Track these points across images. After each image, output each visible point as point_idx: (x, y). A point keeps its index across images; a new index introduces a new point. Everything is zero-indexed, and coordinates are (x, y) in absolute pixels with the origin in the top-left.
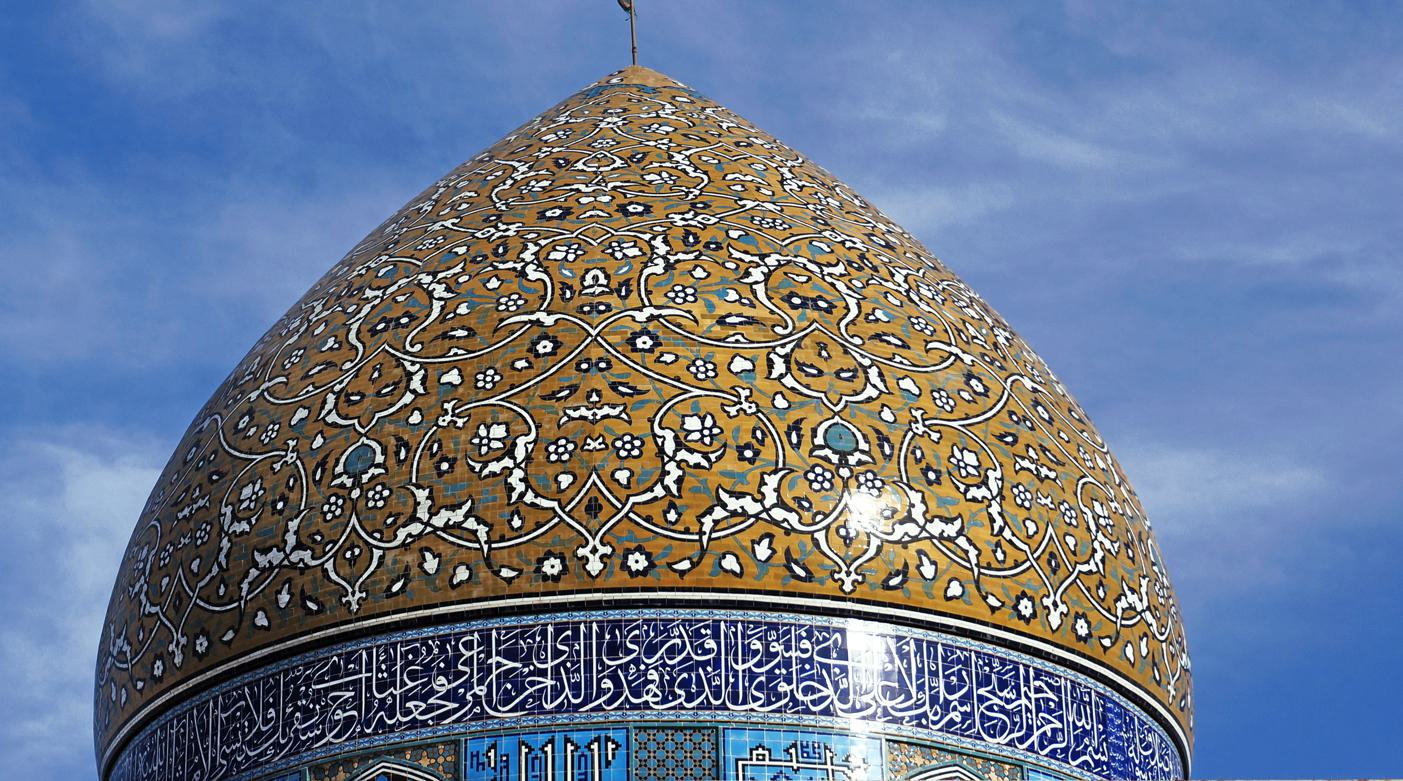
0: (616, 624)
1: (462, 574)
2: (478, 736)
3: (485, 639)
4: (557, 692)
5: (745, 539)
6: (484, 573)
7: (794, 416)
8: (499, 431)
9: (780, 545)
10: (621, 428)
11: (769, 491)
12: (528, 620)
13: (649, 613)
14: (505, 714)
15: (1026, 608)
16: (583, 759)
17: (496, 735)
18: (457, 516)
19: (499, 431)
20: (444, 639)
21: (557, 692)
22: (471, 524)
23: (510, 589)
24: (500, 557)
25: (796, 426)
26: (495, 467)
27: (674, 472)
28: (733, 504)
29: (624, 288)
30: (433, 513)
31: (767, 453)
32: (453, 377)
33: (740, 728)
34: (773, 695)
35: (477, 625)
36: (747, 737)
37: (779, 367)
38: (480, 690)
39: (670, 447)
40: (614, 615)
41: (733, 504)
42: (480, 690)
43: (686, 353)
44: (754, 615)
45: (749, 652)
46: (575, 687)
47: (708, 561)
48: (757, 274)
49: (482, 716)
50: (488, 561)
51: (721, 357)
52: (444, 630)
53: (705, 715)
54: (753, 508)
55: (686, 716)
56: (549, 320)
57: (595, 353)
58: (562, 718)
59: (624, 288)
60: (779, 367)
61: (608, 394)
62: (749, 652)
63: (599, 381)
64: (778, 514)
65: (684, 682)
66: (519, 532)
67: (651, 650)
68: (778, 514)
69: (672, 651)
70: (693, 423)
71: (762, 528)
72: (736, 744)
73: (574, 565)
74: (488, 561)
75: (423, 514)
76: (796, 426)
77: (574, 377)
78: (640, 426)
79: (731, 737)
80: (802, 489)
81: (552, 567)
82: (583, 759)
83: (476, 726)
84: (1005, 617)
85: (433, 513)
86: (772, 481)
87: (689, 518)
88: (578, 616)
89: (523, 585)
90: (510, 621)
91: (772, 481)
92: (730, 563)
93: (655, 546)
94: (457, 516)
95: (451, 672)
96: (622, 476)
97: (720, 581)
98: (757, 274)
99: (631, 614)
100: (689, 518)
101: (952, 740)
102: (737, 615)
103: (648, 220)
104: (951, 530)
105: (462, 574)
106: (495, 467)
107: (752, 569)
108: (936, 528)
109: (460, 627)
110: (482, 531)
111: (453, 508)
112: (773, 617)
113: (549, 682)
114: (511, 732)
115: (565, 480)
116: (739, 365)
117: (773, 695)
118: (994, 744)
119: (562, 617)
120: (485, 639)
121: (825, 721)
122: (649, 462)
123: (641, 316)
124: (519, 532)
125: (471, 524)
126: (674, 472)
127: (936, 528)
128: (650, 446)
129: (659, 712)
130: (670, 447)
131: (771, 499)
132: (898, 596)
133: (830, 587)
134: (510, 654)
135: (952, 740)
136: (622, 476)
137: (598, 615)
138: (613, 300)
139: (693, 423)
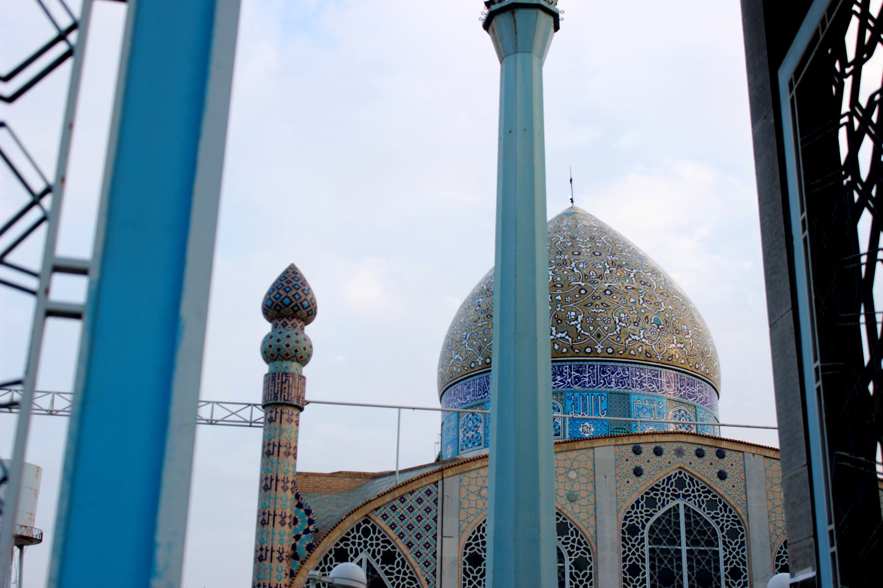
0: (604, 366)
1: (565, 350)
2: (569, 392)
3: (570, 367)
4: (589, 382)
5: (636, 346)
6: (570, 350)
7: (646, 315)
8: (573, 314)
9: (644, 348)
10: (605, 315)
11: (641, 334)
12: (581, 363)
13: (612, 364)
14: (576, 387)
15: (697, 366)
16: (596, 400)
17: (573, 392)
18: (563, 335)
19: (573, 314)
20: (559, 366)
21: (589, 382)
22: (567, 337)
23: (577, 355)
24: (575, 347)
25: (647, 318)
26: (573, 323)
27: (619, 328)
28: (633, 337)
29: (600, 277)
30: (557, 333)
31: (641, 324)
32: (559, 298)
33: (635, 394)
34: (642, 386)
35: (568, 363)
36: (636, 397)
37: (641, 302)
38: (569, 380)
39: (617, 321)
40: (603, 363)
41: (633, 337)
42: (569, 380)
43: (619, 296)
44: (637, 366)
45: (636, 375)
46: (594, 382)
47: (627, 351)
48: (632, 275)
49: (570, 387)
50: (572, 347)
51: (627, 298)
52: (559, 364)
53: (626, 391)
54: (638, 338)
55: (622, 391)
56: (583, 284)
57: (596, 295)
58: (591, 389)
59: (600, 277)
60: (641, 302)
61: (601, 306)
62: (636, 375)
63: (598, 302)
64: (644, 340)
65: (621, 382)
66: (580, 341)
67: (613, 373)
68: (644, 340)
69: (618, 374)
70: (622, 315)
71: (640, 344)
72: (633, 398)
73: (594, 350)
74: (572, 347)
75: (554, 333)
76: (647, 318)
77: (592, 301)
78: (610, 315)
79: (633, 397)
80: (649, 334)
81: (588, 350)
82: (596, 400)
83: (568, 389)
84: (693, 369)
85: (557, 333)
86: (642, 331)
87: (623, 340)
88: (594, 363)
89: (581, 354)
90: (577, 363)
91: (642, 331)
92: (632, 352)
93: (615, 347)
94: (563, 335)
95: (561, 374)
96: (606, 328)
97: (630, 357)
98: (632, 275)
99: (608, 363)
100: (623, 340)
101: (681, 399)
102: (633, 365)
103: (601, 258)
104: (682, 346)
105: (565, 350)
106: (573, 323)
107: (638, 354)
108: (679, 345)
109: (563, 363)
110: (570, 340)
111: (562, 333)
112: (641, 366)
113: (587, 380)
114: (577, 391)
115: (591, 328)
116: (632, 300)
117: (642, 386)
118: (690, 401)
119: (590, 363)
120: (570, 367)
121: (654, 394)
122: (612, 325)
123: (607, 285)
124: (580, 341)
125: (567, 337)
126: (619, 328)
127: (679, 345)
128: (613, 322)
129: (615, 389)
130: (617, 321)
131: (642, 336)
132: (670, 363)
133: (655, 360)
134: (577, 371)
135: (681, 399)
136: (606, 328)
137: (599, 363)
138: (598, 280)
139: (622, 315)
